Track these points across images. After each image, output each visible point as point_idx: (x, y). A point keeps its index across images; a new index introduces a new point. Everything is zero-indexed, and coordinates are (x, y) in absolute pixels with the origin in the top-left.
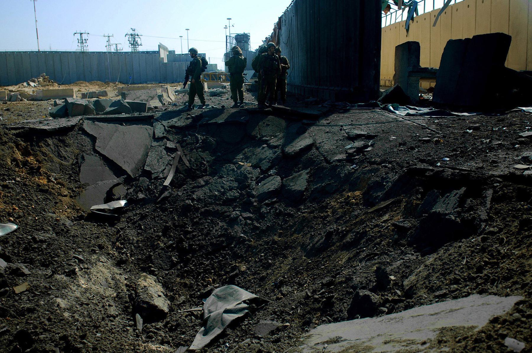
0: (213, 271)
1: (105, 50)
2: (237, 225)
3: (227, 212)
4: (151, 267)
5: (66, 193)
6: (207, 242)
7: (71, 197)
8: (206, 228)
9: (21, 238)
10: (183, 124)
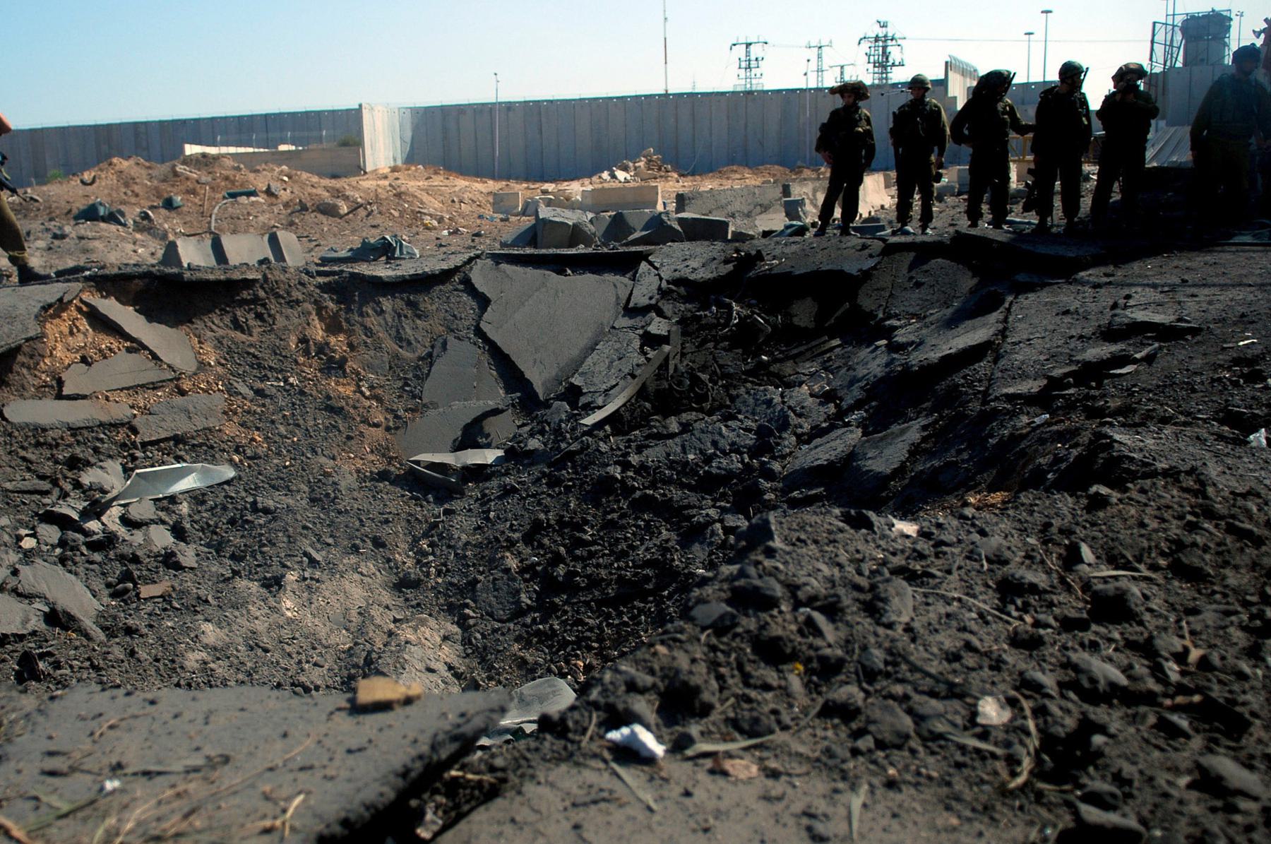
0: (595, 645)
1: (799, 83)
2: (701, 543)
3: (694, 507)
4: (467, 606)
5: (380, 418)
6: (611, 574)
7: (388, 429)
8: (626, 539)
9: (232, 498)
10: (710, 276)
